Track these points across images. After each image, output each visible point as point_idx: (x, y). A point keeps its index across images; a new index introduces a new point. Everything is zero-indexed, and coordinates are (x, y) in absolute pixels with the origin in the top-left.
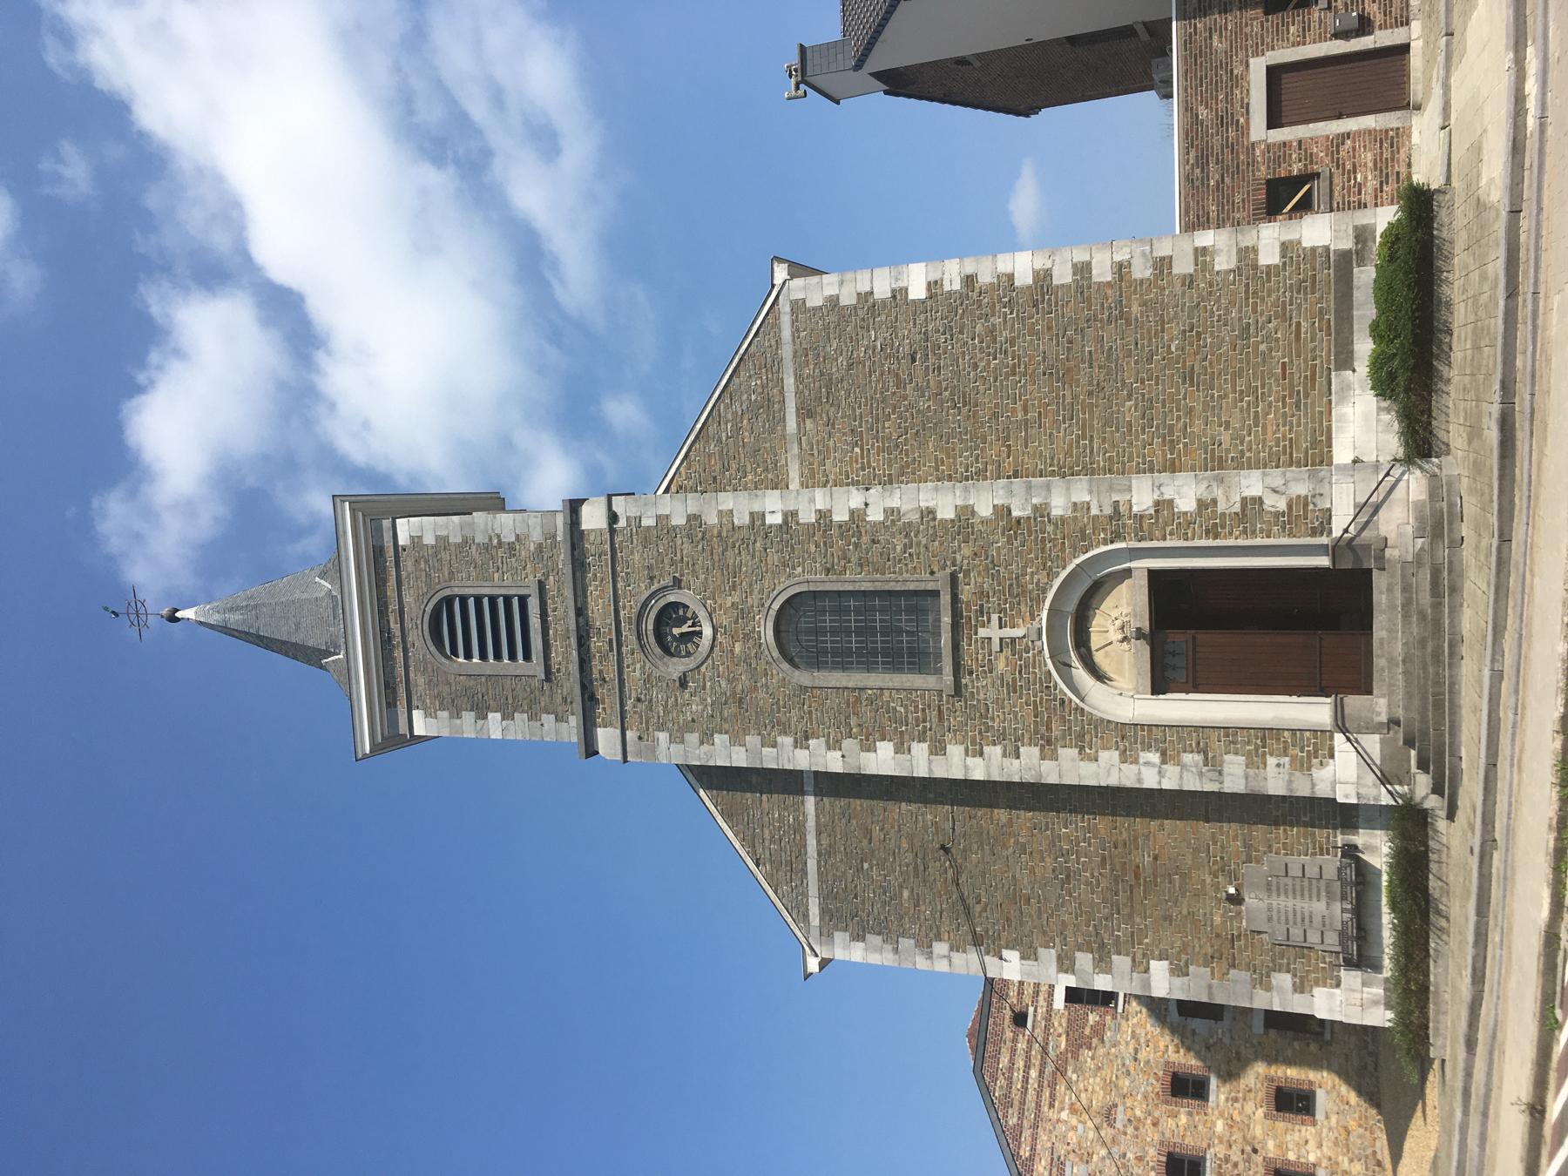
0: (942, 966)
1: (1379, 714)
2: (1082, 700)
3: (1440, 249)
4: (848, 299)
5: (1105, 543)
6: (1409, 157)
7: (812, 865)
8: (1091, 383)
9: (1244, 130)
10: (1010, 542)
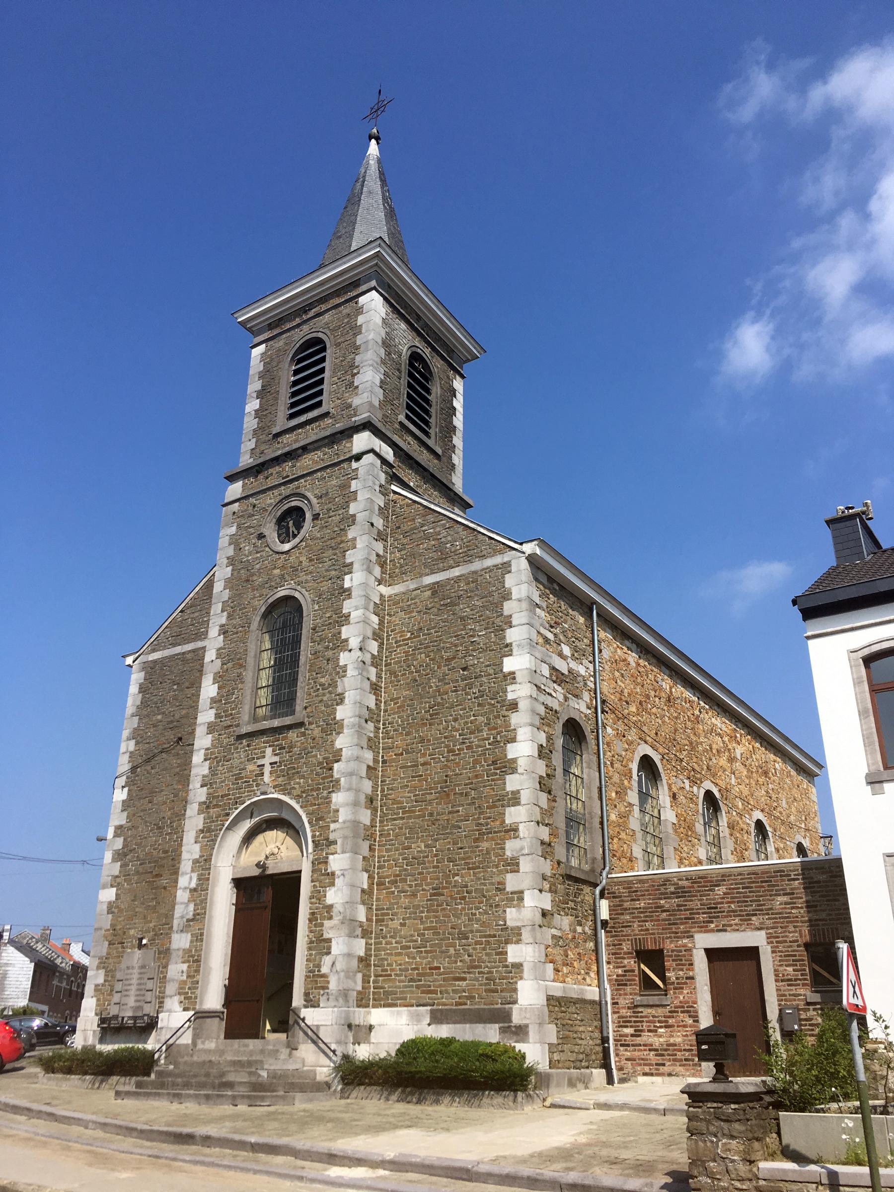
0: (123, 749)
1: (203, 1043)
2: (227, 829)
3: (475, 1096)
4: (508, 607)
5: (313, 836)
6: (677, 1075)
7: (178, 649)
8: (438, 814)
9: (704, 928)
10: (320, 763)
